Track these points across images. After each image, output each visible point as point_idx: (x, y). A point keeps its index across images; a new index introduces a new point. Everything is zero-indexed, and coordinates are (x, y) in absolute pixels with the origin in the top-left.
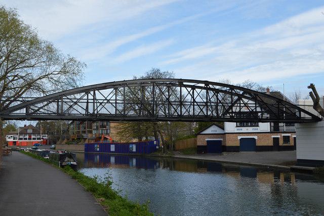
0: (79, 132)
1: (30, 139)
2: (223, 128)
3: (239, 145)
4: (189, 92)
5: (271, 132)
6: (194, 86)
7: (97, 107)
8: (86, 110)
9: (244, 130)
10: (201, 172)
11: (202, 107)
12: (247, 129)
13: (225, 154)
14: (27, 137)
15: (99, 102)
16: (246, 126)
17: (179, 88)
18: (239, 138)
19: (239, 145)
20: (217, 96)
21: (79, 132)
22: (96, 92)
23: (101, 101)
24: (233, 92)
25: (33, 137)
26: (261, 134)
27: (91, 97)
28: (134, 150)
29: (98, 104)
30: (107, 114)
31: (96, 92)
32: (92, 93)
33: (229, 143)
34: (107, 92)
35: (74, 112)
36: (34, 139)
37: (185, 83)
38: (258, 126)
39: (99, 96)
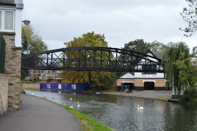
0: (36, 75)
3: (143, 86)
5: (164, 78)
8: (46, 63)
9: (147, 76)
12: (149, 76)
13: (134, 92)
17: (115, 53)
18: (144, 81)
19: (121, 85)
21: (36, 75)
22: (53, 53)
26: (158, 79)
27: (50, 57)
28: (75, 88)
29: (54, 60)
30: (121, 76)
31: (53, 53)
32: (51, 54)
34: (58, 54)
37: (118, 51)
38: (156, 74)
39: (54, 57)
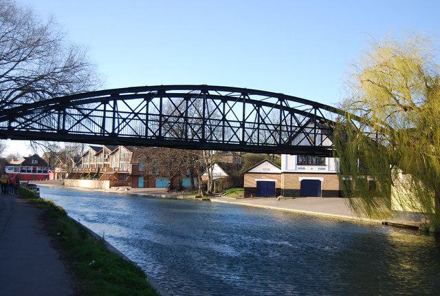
1: (34, 171)
2: (279, 166)
4: (217, 107)
6: (188, 94)
7: (119, 125)
9: (308, 169)
10: (256, 218)
11: (235, 129)
12: (312, 169)
14: (31, 168)
15: (121, 118)
16: (311, 165)
18: (301, 178)
20: (258, 111)
23: (124, 116)
24: (284, 104)
25: (38, 169)
32: (112, 103)
33: (281, 185)
35: (83, 129)
36: (39, 172)
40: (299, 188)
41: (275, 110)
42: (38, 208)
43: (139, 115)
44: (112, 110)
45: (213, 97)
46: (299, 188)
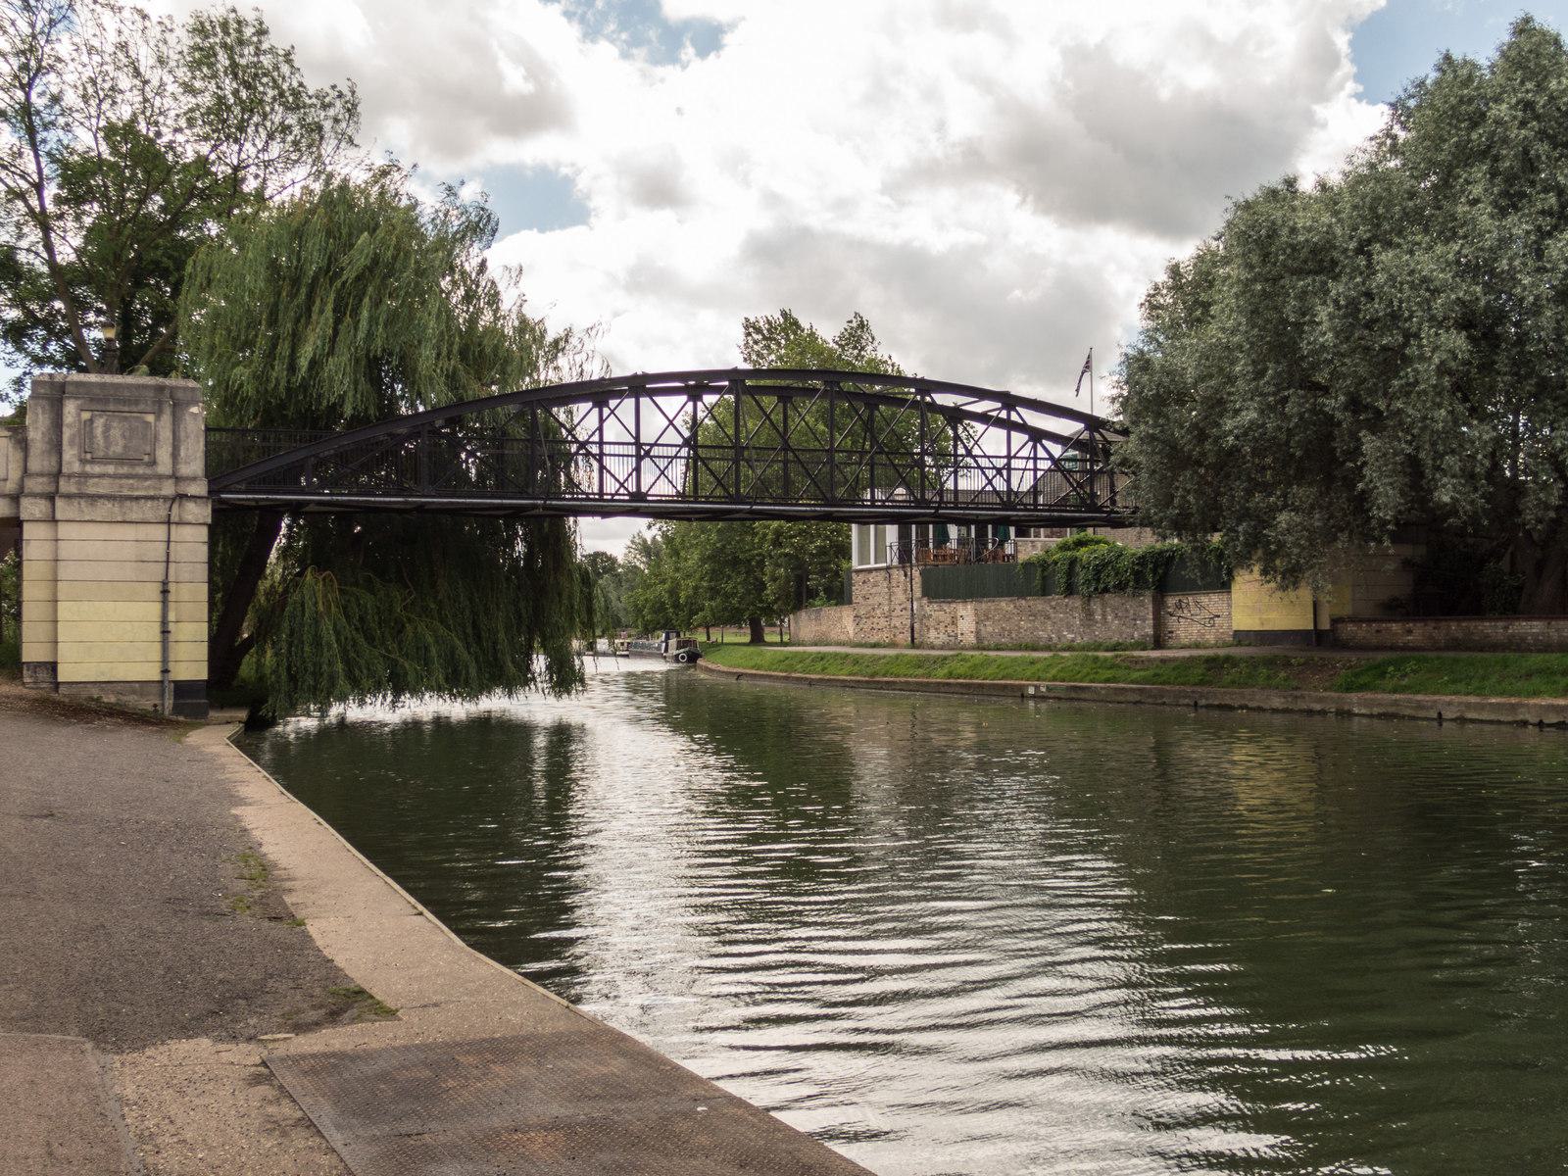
40: (204, 676)
41: (993, 430)
42: (1039, 580)
43: (588, 447)
44: (633, 441)
45: (851, 396)
46: (204, 676)
